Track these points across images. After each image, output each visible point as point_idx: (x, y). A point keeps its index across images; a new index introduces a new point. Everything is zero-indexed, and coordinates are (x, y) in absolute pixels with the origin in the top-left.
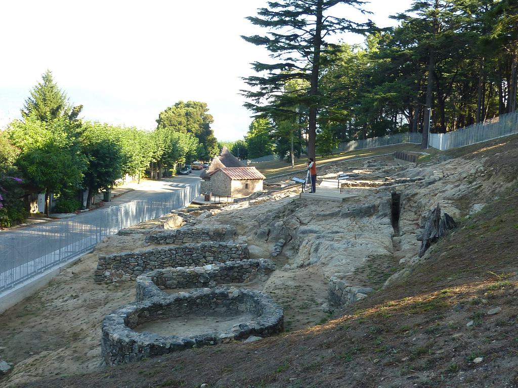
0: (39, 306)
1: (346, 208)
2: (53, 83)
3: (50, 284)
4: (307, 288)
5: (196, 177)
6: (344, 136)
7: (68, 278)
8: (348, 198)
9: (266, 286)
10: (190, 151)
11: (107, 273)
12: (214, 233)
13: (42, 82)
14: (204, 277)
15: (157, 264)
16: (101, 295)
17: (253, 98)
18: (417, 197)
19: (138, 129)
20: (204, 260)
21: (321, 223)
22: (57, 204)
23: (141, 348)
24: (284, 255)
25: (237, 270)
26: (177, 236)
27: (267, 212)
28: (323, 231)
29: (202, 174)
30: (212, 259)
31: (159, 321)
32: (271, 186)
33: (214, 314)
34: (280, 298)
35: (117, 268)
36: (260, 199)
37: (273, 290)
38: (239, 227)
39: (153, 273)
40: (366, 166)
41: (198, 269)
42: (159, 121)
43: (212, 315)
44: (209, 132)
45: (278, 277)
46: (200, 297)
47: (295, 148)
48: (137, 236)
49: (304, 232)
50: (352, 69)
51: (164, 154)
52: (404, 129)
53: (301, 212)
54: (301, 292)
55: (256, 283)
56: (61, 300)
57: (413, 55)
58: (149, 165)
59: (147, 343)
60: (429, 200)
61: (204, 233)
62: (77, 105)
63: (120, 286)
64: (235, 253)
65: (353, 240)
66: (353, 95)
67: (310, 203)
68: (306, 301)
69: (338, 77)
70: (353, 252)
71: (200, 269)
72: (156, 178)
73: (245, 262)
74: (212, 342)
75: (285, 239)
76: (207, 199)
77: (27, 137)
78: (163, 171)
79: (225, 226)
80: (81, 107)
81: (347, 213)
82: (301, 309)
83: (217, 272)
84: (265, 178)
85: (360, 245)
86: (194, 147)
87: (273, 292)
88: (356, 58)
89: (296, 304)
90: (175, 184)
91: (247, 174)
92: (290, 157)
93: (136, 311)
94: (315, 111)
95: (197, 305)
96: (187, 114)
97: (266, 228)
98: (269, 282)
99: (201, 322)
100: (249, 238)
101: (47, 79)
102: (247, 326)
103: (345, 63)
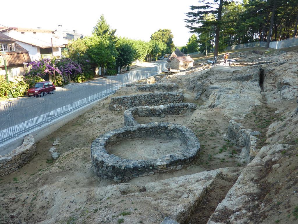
0: (83, 120)
1: (235, 76)
2: (104, 19)
3: (92, 109)
4: (214, 122)
5: (166, 62)
6: (229, 44)
7: (100, 107)
8: (236, 71)
9: (191, 118)
10: (163, 50)
11: (115, 106)
12: (168, 87)
13: (100, 19)
14: (159, 112)
15: (138, 102)
16: (111, 117)
17: (190, 23)
18: (274, 72)
19: (142, 41)
20: (161, 101)
21: (221, 83)
22: (107, 72)
23: (107, 167)
24: (201, 99)
25: (176, 109)
26: (151, 88)
27: (194, 77)
28: (222, 88)
29: (167, 60)
30: (164, 100)
31: (129, 140)
32: (196, 65)
33: (160, 137)
34: (198, 128)
35: (119, 104)
36: (191, 70)
37: (194, 122)
38: (180, 84)
39: (133, 109)
40: (239, 56)
41: (156, 108)
42: (151, 38)
43: (158, 138)
44: (172, 42)
45: (199, 114)
46: (152, 128)
47: (208, 48)
48: (133, 87)
49: (212, 88)
50: (235, 13)
51: (152, 51)
52: (256, 40)
53: (211, 77)
54: (210, 125)
55: (186, 115)
56: (93, 118)
57: (266, 4)
58: (146, 56)
59: (110, 164)
60: (283, 73)
61: (163, 87)
62: (114, 29)
63: (120, 113)
64: (176, 98)
65: (239, 94)
66: (234, 25)
67: (216, 73)
68: (214, 131)
69: (229, 16)
70: (240, 101)
71: (157, 108)
72: (149, 61)
73: (181, 104)
74: (151, 168)
75: (202, 91)
76: (169, 70)
77: (92, 42)
78: (152, 58)
79: (173, 84)
80: (116, 30)
81: (235, 79)
82: (210, 136)
83: (166, 109)
84: (194, 61)
85: (244, 97)
86: (165, 48)
87: (195, 123)
88: (237, 7)
89: (208, 133)
90: (157, 64)
91: (185, 59)
92: (205, 52)
93: (115, 135)
94: (216, 33)
95: (150, 132)
96: (163, 34)
97: (192, 85)
98: (193, 116)
99: (152, 142)
100: (184, 90)
101: (102, 18)
102: (175, 157)
103: (232, 10)
